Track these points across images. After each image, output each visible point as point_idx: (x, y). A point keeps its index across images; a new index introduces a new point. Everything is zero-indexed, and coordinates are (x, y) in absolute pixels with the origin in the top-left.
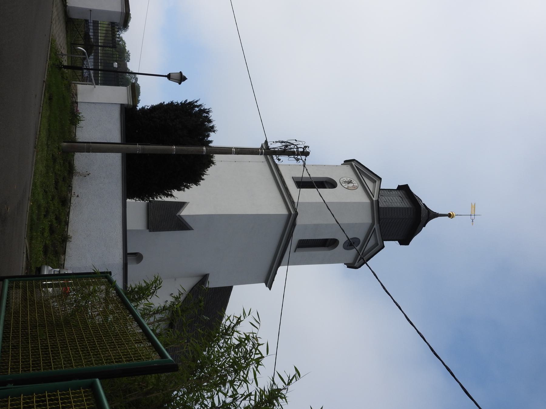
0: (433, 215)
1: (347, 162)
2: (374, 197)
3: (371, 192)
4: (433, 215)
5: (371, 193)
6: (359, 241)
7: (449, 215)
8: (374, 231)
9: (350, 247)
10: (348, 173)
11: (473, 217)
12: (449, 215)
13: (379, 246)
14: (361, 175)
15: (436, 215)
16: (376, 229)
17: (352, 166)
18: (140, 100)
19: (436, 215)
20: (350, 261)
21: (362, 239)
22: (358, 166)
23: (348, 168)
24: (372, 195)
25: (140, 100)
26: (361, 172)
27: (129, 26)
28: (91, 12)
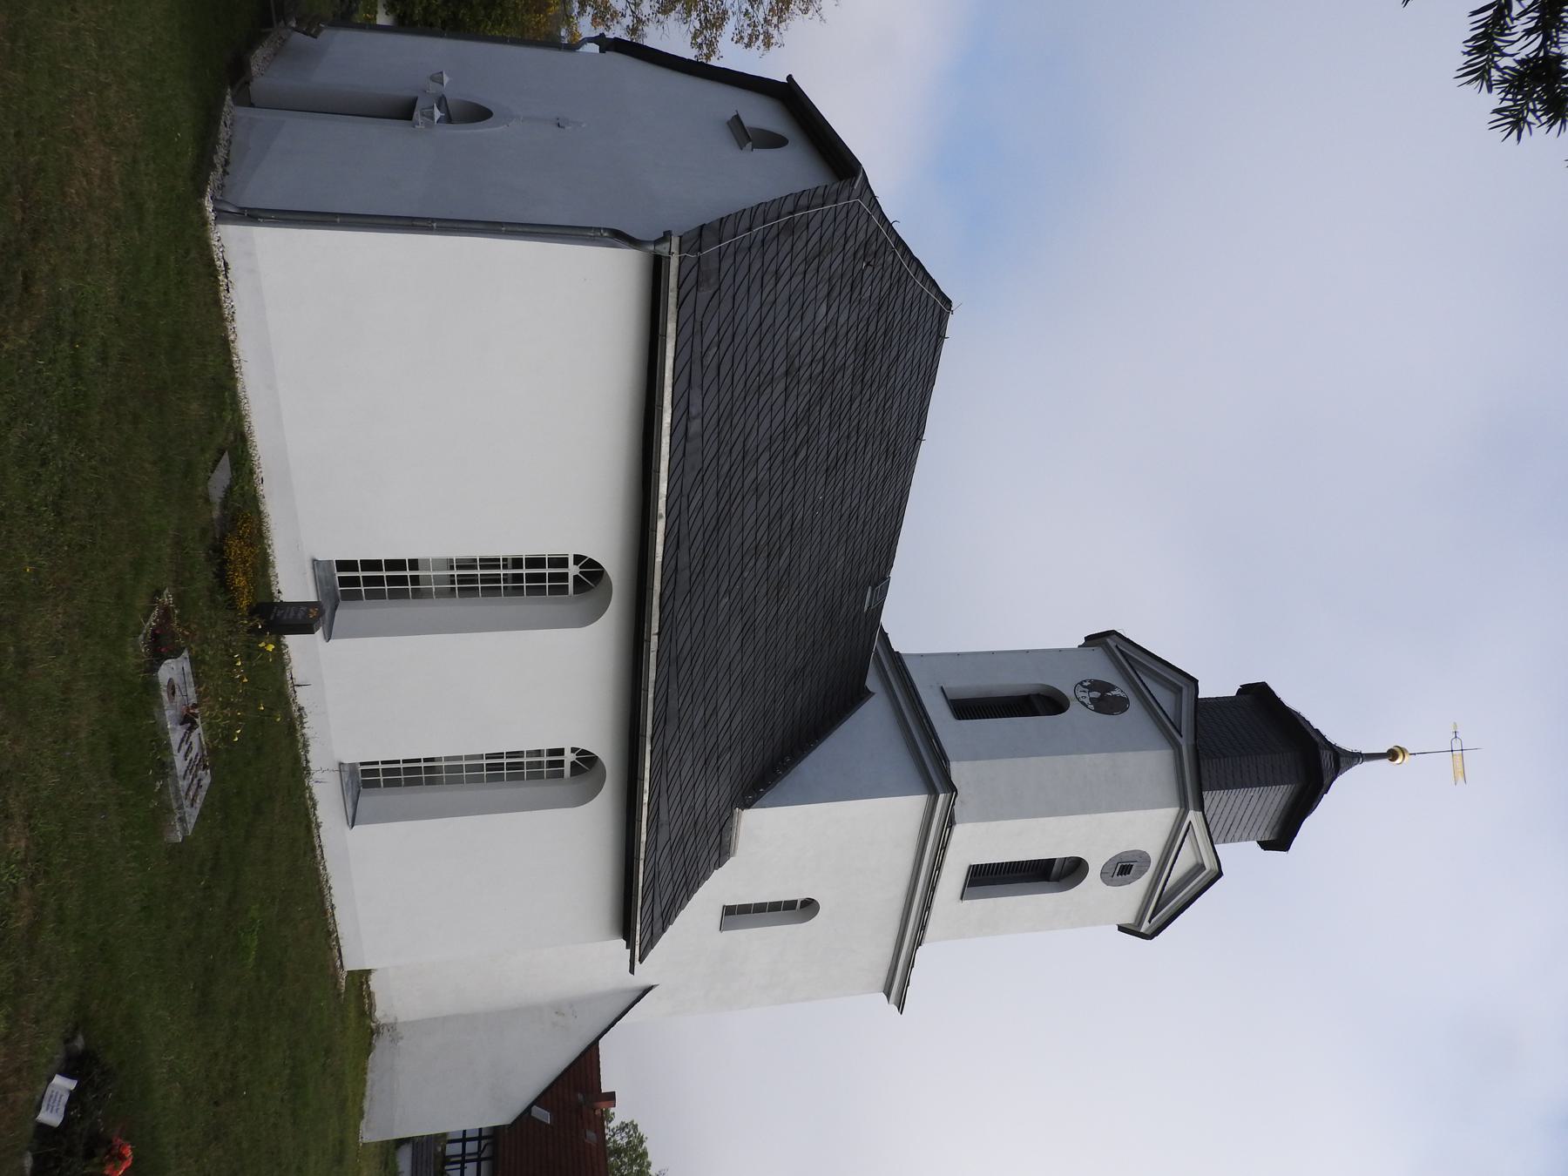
0: (1343, 759)
1: (1092, 640)
2: (1181, 736)
3: (1170, 720)
4: (1343, 759)
5: (1170, 720)
6: (1148, 860)
7: (1392, 755)
8: (1190, 830)
9: (1120, 876)
10: (1101, 668)
11: (1457, 746)
12: (1392, 755)
13: (1208, 873)
14: (1136, 673)
15: (1357, 757)
16: (1194, 823)
17: (1107, 649)
18: (611, 1097)
19: (1357, 757)
20: (1128, 918)
21: (1155, 856)
22: (1124, 650)
23: (1097, 653)
24: (1175, 728)
25: (611, 1097)
26: (1136, 666)
27: (318, 826)
28: (1386, 761)
